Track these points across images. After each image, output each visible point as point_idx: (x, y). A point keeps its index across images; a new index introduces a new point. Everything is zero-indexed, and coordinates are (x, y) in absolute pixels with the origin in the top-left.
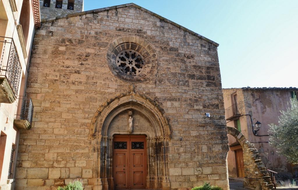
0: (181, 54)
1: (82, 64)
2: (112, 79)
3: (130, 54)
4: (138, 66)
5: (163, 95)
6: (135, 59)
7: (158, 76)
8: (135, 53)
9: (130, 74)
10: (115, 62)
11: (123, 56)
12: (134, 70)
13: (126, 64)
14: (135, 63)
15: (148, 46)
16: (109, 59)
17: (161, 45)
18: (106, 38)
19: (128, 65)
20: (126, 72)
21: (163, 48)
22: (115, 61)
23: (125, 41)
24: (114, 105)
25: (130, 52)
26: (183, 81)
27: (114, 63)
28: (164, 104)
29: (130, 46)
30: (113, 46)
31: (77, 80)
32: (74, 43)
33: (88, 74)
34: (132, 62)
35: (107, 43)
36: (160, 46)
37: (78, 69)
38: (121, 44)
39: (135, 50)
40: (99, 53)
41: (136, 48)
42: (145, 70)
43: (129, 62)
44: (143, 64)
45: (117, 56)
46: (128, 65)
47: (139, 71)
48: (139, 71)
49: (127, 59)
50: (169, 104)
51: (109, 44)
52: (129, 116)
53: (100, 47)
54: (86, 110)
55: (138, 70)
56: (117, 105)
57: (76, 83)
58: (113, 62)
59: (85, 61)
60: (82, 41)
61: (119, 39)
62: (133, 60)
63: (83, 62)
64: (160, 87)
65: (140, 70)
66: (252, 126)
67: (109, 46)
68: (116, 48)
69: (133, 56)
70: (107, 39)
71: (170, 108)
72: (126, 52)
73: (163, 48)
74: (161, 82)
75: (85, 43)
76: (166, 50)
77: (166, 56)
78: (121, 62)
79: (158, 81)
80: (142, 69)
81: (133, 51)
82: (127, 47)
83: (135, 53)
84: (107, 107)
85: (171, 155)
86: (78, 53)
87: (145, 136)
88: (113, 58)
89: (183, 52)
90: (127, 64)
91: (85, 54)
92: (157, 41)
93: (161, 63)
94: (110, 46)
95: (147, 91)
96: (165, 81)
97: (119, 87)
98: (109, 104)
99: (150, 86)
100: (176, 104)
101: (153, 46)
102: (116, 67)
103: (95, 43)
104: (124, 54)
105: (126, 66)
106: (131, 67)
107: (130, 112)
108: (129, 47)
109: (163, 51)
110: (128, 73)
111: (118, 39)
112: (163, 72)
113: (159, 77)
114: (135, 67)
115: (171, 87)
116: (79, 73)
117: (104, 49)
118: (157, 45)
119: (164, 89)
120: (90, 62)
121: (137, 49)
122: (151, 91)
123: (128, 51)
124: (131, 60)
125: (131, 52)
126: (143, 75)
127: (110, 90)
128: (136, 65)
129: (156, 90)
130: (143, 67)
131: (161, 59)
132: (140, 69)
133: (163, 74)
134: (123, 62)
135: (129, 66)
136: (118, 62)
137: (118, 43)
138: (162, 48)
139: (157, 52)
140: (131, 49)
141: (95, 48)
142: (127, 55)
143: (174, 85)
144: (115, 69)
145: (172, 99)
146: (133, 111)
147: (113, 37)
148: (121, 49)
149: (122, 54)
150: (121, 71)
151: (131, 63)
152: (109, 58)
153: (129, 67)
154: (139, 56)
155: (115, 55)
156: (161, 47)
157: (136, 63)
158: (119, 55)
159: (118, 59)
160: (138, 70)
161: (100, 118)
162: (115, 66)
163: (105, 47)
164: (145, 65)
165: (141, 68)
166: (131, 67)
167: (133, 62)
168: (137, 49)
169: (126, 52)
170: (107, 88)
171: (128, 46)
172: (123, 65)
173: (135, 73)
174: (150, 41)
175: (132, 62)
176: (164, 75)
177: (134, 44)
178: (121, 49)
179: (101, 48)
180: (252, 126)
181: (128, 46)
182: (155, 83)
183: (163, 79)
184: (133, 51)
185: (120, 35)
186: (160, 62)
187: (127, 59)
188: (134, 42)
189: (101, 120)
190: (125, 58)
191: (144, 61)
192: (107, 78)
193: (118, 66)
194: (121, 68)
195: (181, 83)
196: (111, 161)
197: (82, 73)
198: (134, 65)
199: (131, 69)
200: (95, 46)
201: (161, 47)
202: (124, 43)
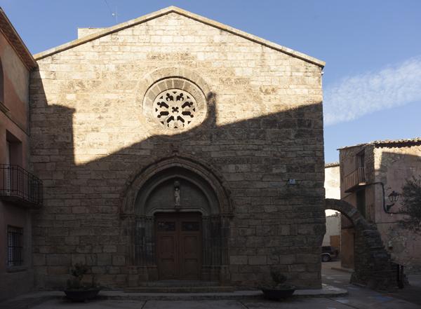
0: (254, 87)
1: (100, 118)
3: (175, 96)
5: (222, 156)
8: (182, 95)
11: (164, 100)
18: (133, 73)
24: (151, 173)
26: (255, 132)
28: (224, 169)
31: (96, 141)
32: (87, 86)
33: (110, 130)
35: (136, 82)
37: (96, 126)
38: (157, 81)
40: (124, 99)
44: (194, 110)
50: (232, 168)
52: (176, 188)
53: (125, 89)
54: (111, 181)
56: (153, 173)
57: (95, 145)
59: (104, 112)
60: (98, 82)
63: (102, 115)
64: (217, 143)
67: (137, 86)
71: (234, 173)
75: (102, 86)
81: (179, 92)
83: (182, 95)
84: (140, 176)
85: (232, 239)
86: (92, 102)
87: (200, 214)
88: (147, 104)
89: (257, 84)
91: (104, 103)
92: (215, 69)
95: (197, 149)
97: (156, 147)
98: (143, 170)
99: (202, 143)
100: (243, 167)
103: (117, 83)
104: (165, 96)
107: (177, 182)
111: (151, 72)
114: (182, 116)
115: (236, 142)
116: (98, 131)
117: (131, 91)
118: (214, 75)
119: (224, 146)
120: (111, 113)
122: (203, 149)
123: (171, 92)
125: (175, 93)
127: (143, 153)
129: (211, 148)
136: (157, 110)
141: (117, 91)
143: (240, 140)
145: (236, 161)
146: (183, 182)
149: (162, 98)
150: (161, 124)
151: (175, 110)
161: (130, 192)
170: (138, 150)
179: (127, 91)
182: (211, 137)
189: (133, 195)
195: (253, 134)
196: (152, 246)
197: (103, 130)
200: (117, 88)
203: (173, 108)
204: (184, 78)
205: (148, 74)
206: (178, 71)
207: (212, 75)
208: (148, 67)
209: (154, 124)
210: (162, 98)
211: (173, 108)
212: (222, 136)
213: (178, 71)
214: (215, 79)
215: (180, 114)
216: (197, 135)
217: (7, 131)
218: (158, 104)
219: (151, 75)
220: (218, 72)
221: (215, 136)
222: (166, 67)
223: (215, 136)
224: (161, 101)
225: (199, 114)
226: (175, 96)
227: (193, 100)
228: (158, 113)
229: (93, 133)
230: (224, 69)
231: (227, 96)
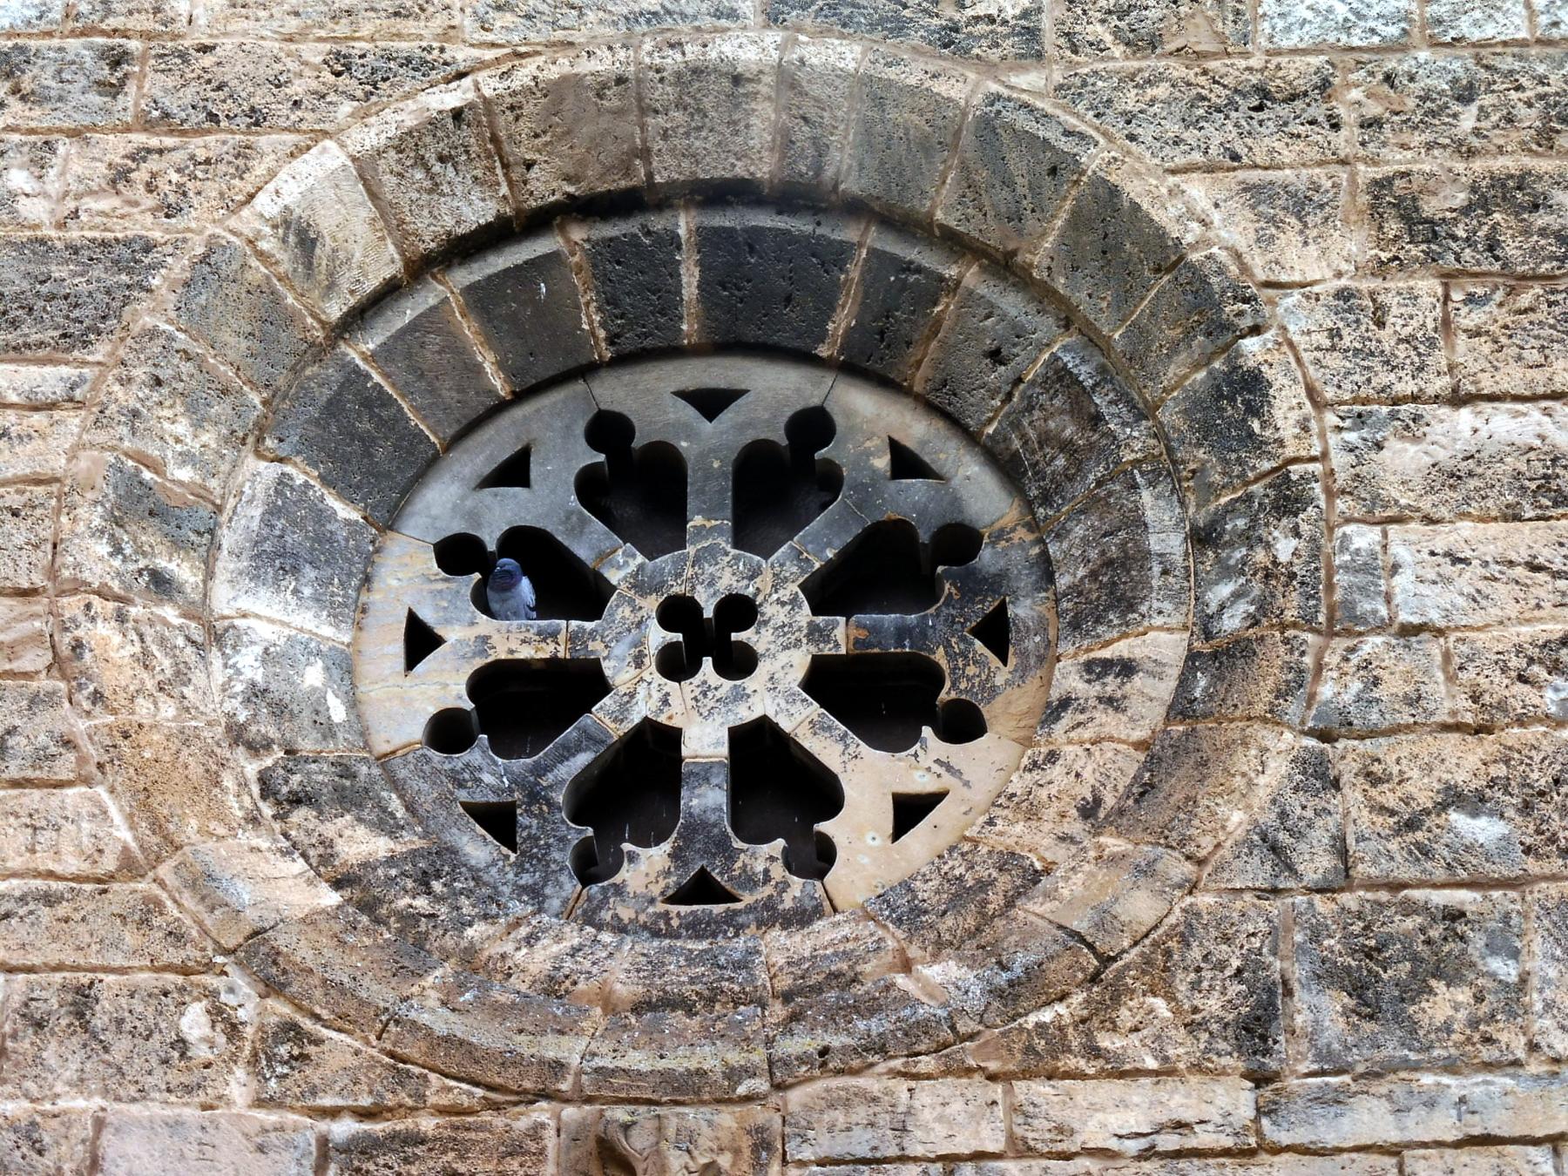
2: (194, 1022)
3: (708, 446)
4: (884, 696)
6: (820, 541)
7: (1316, 863)
8: (813, 426)
9: (701, 889)
10: (345, 667)
11: (548, 502)
12: (780, 787)
13: (608, 668)
14: (815, 634)
15: (1077, 221)
16: (161, 584)
17: (1395, 160)
18: (116, 147)
19: (638, 693)
20: (593, 866)
21: (1440, 204)
22: (336, 634)
23: (545, 186)
25: (689, 413)
27: (314, 676)
29: (690, 280)
30: (270, 316)
34: (740, 610)
35: (134, 257)
36: (1381, 185)
39: (803, 357)
41: (827, 308)
42: (1012, 783)
43: (658, 636)
44: (996, 631)
45: (388, 519)
46: (638, 693)
47: (909, 811)
48: (909, 811)
49: (622, 566)
51: (178, 267)
55: (867, 775)
58: (267, 656)
61: (407, 144)
62: (777, 582)
65: (920, 783)
66: (1458, 1145)
68: (359, 350)
69: (781, 481)
70: (119, 177)
72: (608, 430)
73: (1430, 207)
74: (1416, 989)
76: (1511, 248)
77: (1512, 378)
78: (480, 637)
79: (1329, 975)
80: (982, 763)
81: (772, 392)
82: (610, 302)
83: (813, 426)
88: (275, 562)
90: (618, 672)
92: (1300, 70)
93: (1399, 551)
94: (194, 318)
96: (1507, 970)
101: (1198, 190)
102: (336, 749)
104: (564, 458)
105: (609, 719)
106: (705, 742)
108: (669, 303)
109: (1447, 278)
110: (647, 868)
111: (369, 137)
112: (1465, 762)
113: (1342, 878)
114: (802, 720)
117: (49, 378)
118: (1288, 156)
121: (841, 322)
123: (652, 400)
124: (713, 570)
125: (710, 402)
126: (984, 885)
128: (825, 682)
130: (1009, 707)
131: (1402, 461)
132: (925, 762)
133: (1453, 798)
134: (519, 639)
135: (672, 717)
136: (420, 641)
137: (389, 218)
138: (1409, 214)
139: (1300, 320)
140: (726, 343)
142: (637, 485)
144: (296, 800)
147: (257, 118)
148: (488, 362)
149: (514, 472)
150: (477, 847)
151: (708, 639)
152: (184, 571)
153: (655, 747)
154: (906, 463)
155: (346, 512)
156: (1395, 205)
157: (842, 635)
158: (443, 504)
159: (408, 576)
160: (867, 775)
162: (328, 731)
163: (73, 340)
164: (1047, 658)
165: (963, 724)
166: (705, 742)
167: (771, 611)
168: (841, 322)
169: (608, 430)
171: (636, 279)
172: (523, 705)
173: (816, 858)
174: (1130, 100)
175: (740, 610)
176: (1483, 830)
177: (765, 220)
178: (488, 362)
180: (1458, 1145)
181: (636, 279)
182: (1256, 1029)
183: (1454, 915)
184: (772, 392)
185: (418, 65)
186: (1364, 538)
187: (622, 566)
188: (763, 168)
190: (588, 540)
191: (1025, 581)
192: (82, 1001)
193: (415, 730)
194: (488, 770)
198: (777, 691)
199: (704, 773)
201: (1395, 205)
202: (538, 221)
203: (677, 612)
204: (855, 208)
205: (329, 158)
206: (762, 120)
207: (1267, 142)
208: (341, 64)
209: (359, 843)
210: (514, 472)
211: (677, 612)
212: (1445, 1004)
213: (762, 120)
214: (1302, 204)
215: (777, 691)
216: (1012, 996)
217: (896, 836)
218: (457, 554)
219: (364, 169)
220: (1353, 99)
221: (1319, 1012)
222: (602, 64)
223: (1319, 1012)
224: (497, 515)
225: (1068, 679)
226: (708, 446)
227: (980, 494)
228: (445, 684)
229: (1153, 695)
230: (1432, 68)
231: (1506, 426)
